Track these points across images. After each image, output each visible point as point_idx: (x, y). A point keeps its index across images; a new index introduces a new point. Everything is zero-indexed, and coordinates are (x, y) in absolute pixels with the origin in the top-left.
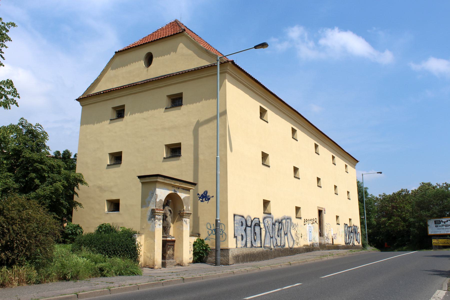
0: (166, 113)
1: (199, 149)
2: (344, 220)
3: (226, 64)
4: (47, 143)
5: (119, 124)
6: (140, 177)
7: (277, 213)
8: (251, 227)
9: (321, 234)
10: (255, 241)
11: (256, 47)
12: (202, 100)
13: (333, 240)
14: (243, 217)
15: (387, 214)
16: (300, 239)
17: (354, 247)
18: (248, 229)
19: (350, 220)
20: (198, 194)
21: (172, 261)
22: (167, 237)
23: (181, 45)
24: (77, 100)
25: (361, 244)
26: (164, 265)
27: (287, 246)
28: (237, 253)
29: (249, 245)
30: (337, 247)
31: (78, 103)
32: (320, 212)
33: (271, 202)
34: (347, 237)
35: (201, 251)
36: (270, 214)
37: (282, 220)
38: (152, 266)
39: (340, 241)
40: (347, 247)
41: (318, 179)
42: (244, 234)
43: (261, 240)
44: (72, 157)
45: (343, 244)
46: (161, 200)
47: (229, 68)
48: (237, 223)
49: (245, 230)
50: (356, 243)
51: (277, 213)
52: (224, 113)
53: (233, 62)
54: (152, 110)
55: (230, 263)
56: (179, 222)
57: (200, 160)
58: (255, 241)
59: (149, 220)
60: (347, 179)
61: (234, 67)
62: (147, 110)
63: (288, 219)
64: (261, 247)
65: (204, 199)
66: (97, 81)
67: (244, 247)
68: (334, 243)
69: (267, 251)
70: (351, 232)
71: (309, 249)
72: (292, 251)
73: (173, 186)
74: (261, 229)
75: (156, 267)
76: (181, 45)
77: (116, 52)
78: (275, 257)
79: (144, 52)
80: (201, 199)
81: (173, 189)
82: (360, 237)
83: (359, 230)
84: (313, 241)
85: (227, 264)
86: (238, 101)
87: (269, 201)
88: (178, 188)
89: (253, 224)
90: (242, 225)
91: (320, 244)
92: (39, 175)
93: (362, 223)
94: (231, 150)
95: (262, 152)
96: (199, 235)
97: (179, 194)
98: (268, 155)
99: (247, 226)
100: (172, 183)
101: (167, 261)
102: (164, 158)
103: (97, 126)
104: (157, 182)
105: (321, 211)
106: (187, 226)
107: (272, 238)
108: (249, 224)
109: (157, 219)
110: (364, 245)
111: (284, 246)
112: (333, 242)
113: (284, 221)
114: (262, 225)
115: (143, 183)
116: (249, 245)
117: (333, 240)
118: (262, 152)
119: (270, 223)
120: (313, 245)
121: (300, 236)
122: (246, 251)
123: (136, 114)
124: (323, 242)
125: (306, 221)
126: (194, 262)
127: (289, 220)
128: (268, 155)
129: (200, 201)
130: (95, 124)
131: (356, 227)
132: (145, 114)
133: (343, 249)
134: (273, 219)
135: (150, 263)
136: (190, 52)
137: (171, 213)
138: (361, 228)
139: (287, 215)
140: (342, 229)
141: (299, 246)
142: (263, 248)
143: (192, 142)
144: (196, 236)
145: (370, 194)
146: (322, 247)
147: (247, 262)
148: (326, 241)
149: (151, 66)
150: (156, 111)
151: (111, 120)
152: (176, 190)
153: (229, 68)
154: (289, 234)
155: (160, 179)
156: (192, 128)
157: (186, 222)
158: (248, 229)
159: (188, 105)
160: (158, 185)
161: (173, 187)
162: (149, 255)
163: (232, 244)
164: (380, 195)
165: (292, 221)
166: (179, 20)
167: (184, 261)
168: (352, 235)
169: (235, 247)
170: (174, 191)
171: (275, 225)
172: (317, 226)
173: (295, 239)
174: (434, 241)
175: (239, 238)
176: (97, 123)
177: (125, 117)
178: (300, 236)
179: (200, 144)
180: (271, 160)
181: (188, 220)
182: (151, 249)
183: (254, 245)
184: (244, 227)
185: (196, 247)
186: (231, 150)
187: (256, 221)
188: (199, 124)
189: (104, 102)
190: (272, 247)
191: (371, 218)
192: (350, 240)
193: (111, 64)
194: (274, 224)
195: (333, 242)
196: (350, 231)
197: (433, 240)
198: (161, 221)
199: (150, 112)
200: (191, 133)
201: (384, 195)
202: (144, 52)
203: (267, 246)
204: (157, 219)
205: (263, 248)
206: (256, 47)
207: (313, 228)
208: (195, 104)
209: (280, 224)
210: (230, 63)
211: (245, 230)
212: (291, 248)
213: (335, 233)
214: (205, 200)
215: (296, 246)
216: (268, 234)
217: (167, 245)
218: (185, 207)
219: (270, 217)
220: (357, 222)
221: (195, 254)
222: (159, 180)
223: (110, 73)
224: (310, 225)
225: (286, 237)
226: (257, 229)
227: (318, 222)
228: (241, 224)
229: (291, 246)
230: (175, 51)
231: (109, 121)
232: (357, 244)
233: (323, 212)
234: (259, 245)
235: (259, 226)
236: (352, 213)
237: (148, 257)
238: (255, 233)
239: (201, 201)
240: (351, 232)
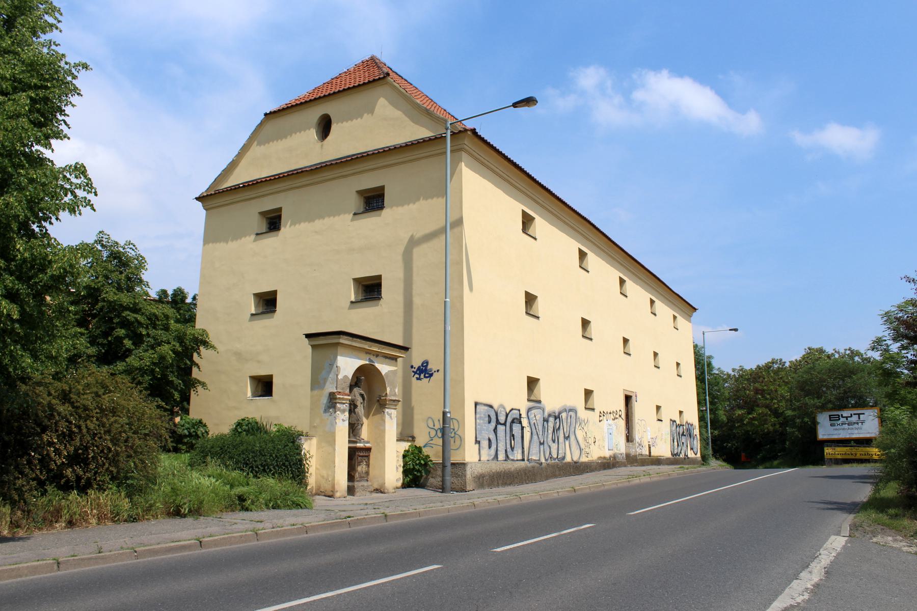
0: (355, 222)
1: (414, 287)
2: (670, 413)
3: (461, 135)
4: (145, 276)
5: (272, 241)
6: (308, 336)
7: (551, 400)
8: (505, 424)
9: (629, 438)
10: (512, 449)
11: (515, 105)
12: (418, 199)
13: (650, 448)
14: (491, 407)
15: (746, 402)
16: (592, 446)
17: (687, 460)
18: (501, 428)
19: (681, 412)
20: (412, 367)
21: (365, 484)
22: (355, 442)
23: (382, 101)
24: (197, 199)
25: (699, 455)
26: (351, 491)
27: (568, 459)
29: (501, 456)
30: (658, 461)
31: (199, 204)
32: (628, 399)
33: (541, 381)
34: (676, 443)
35: (417, 467)
36: (539, 402)
37: (560, 413)
38: (331, 494)
39: (663, 450)
40: (675, 460)
42: (492, 437)
43: (523, 448)
46: (346, 377)
47: (467, 142)
48: (480, 418)
49: (495, 430)
50: (691, 454)
51: (551, 400)
52: (459, 222)
53: (474, 131)
54: (329, 216)
55: (468, 489)
56: (378, 417)
57: (415, 307)
58: (512, 449)
59: (325, 411)
60: (676, 339)
61: (476, 140)
62: (321, 217)
63: (570, 410)
64: (523, 460)
65: (422, 376)
66: (233, 166)
67: (493, 459)
68: (652, 454)
69: (533, 467)
70: (683, 435)
71: (608, 464)
72: (578, 468)
73: (368, 352)
74: (523, 428)
75: (338, 494)
76: (382, 101)
77: (266, 114)
78: (547, 478)
79: (314, 114)
80: (417, 376)
81: (368, 356)
82: (697, 444)
83: (696, 432)
84: (615, 451)
85: (463, 490)
86: (482, 200)
88: (377, 355)
89: (509, 420)
90: (489, 422)
91: (628, 456)
92: (132, 331)
93: (702, 419)
94: (471, 289)
95: (583, 319)
96: (413, 438)
97: (377, 365)
98: (536, 297)
100: (366, 346)
101: (356, 484)
102: (352, 302)
103: (233, 245)
104: (338, 344)
106: (391, 421)
107: (543, 444)
108: (502, 419)
109: (339, 410)
110: (704, 458)
111: (564, 458)
112: (650, 453)
113: (564, 415)
114: (525, 422)
115: (313, 347)
116: (501, 456)
117: (650, 448)
118: (583, 319)
119: (539, 417)
120: (614, 457)
121: (591, 441)
122: (496, 467)
123: (302, 224)
124: (632, 452)
125: (602, 414)
126: (405, 486)
127: (572, 413)
129: (414, 379)
130: (230, 243)
132: (318, 224)
134: (544, 411)
135: (326, 487)
136: (398, 113)
137: (364, 399)
138: (700, 427)
139: (570, 404)
140: (666, 427)
141: (590, 459)
142: (526, 461)
143: (400, 274)
144: (408, 441)
145: (717, 367)
146: (632, 460)
147: (498, 486)
148: (639, 451)
149: (329, 138)
150: (337, 218)
151: (257, 234)
152: (373, 358)
153: (467, 142)
154: (572, 437)
155: (344, 340)
156: (401, 249)
157: (390, 415)
158: (501, 428)
159: (394, 208)
160: (339, 348)
161: (367, 353)
162: (324, 473)
163: (472, 455)
164: (734, 370)
165: (579, 414)
167: (386, 485)
168: (683, 439)
169: (477, 459)
170: (370, 360)
171: (547, 421)
172: (622, 423)
173: (583, 446)
174: (828, 451)
175: (485, 443)
176: (232, 241)
177: (282, 229)
178: (591, 441)
179: (415, 278)
180: (540, 306)
181: (393, 412)
182: (329, 463)
183: (511, 457)
184: (493, 424)
185: (407, 459)
186: (471, 289)
187: (515, 414)
188: (413, 243)
189: (245, 202)
190: (543, 460)
191: (717, 409)
193: (256, 136)
194: (546, 420)
196: (681, 432)
198: (347, 414)
199: (328, 221)
200: (400, 258)
201: (742, 370)
202: (314, 114)
203: (534, 458)
204: (339, 410)
205: (526, 461)
206: (515, 105)
207: (615, 428)
208: (406, 207)
209: (558, 420)
211: (495, 430)
212: (576, 463)
213: (654, 436)
214: (425, 377)
215: (584, 459)
216: (535, 437)
217: (358, 456)
218: (388, 389)
219: (539, 408)
220: (692, 416)
221: (406, 472)
222: (342, 341)
223: (256, 150)
224: (611, 422)
225: (567, 443)
226: (516, 428)
227: (623, 416)
228: (487, 419)
229: (575, 459)
230: (371, 111)
231: (253, 237)
233: (634, 398)
234: (520, 457)
235: (520, 423)
236: (684, 402)
237: (323, 477)
238: (513, 436)
239: (418, 379)
240: (683, 435)
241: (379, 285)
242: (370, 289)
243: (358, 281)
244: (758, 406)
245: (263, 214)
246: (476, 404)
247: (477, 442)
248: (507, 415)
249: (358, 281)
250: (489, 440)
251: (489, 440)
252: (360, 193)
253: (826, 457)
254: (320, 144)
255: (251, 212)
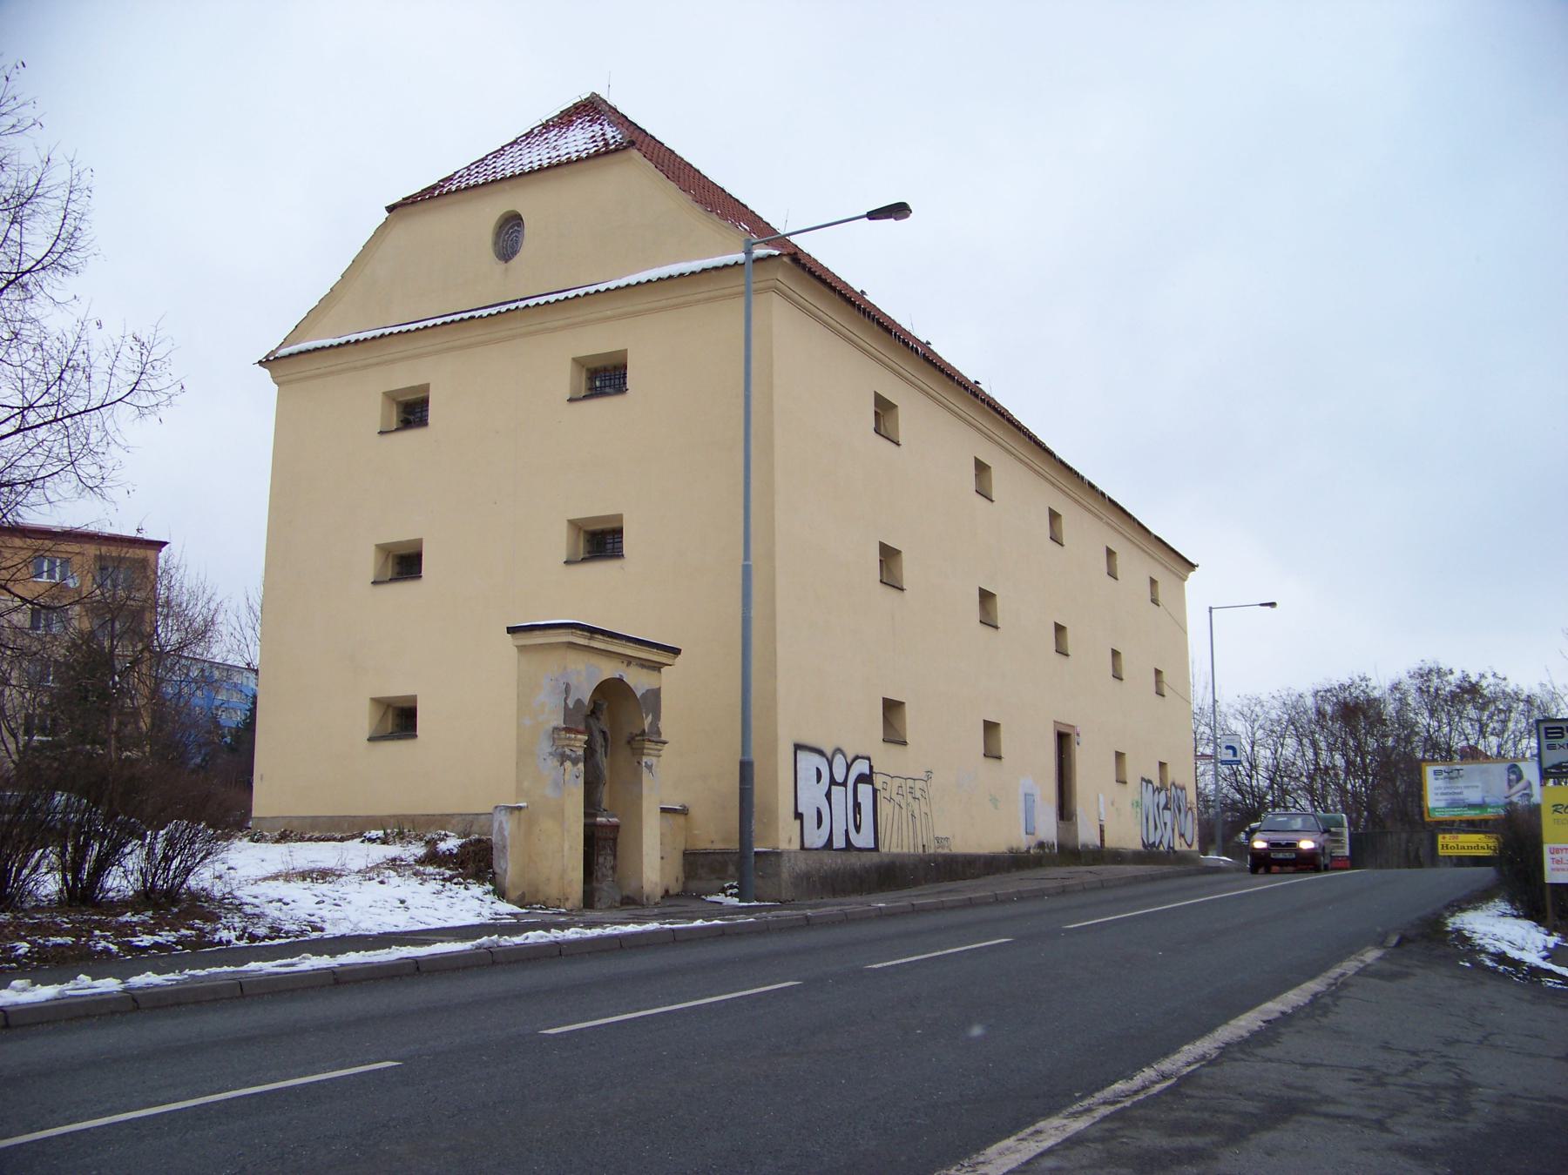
2: (1141, 766)
6: (511, 630)
8: (844, 784)
9: (1065, 810)
10: (858, 828)
11: (873, 215)
13: (1102, 831)
18: (837, 791)
19: (1162, 765)
28: (804, 867)
30: (1118, 857)
31: (265, 373)
39: (1126, 834)
41: (1059, 629)
44: (1390, 709)
45: (1140, 847)
46: (579, 702)
49: (828, 795)
50: (1179, 845)
58: (858, 828)
68: (1107, 844)
70: (1166, 807)
77: (390, 209)
79: (490, 210)
87: (903, 703)
90: (819, 779)
95: (881, 544)
99: (833, 782)
105: (1068, 735)
112: (1102, 840)
117: (1102, 831)
118: (881, 544)
128: (898, 552)
131: (1183, 789)
133: (1136, 863)
158: (837, 791)
166: (604, 96)
168: (1167, 815)
169: (796, 846)
174: (1444, 840)
175: (810, 820)
180: (909, 570)
192: (1159, 832)
195: (1102, 840)
197: (1440, 837)
198: (581, 766)
202: (490, 210)
206: (873, 215)
210: (785, 259)
211: (828, 795)
232: (1185, 848)
233: (1074, 737)
240: (1166, 807)
241: (618, 532)
242: (601, 541)
243: (384, 549)
244: (1396, 791)
245: (390, 396)
246: (798, 747)
247: (799, 816)
248: (848, 767)
249: (384, 549)
250: (818, 771)
251: (818, 771)
252: (578, 361)
253: (1441, 852)
254: (501, 265)
255: (364, 397)
